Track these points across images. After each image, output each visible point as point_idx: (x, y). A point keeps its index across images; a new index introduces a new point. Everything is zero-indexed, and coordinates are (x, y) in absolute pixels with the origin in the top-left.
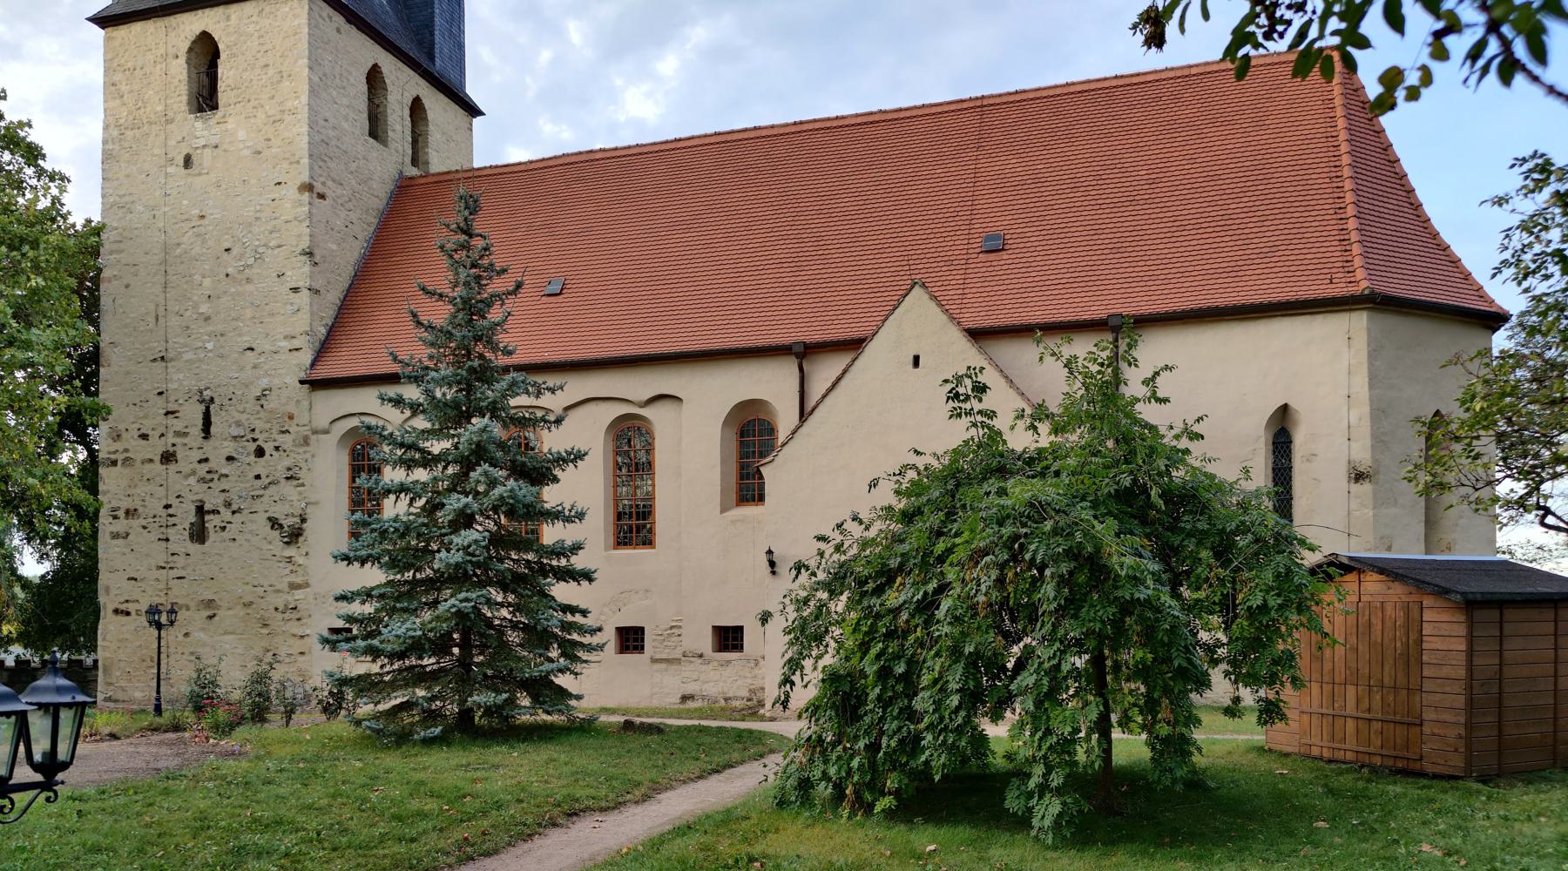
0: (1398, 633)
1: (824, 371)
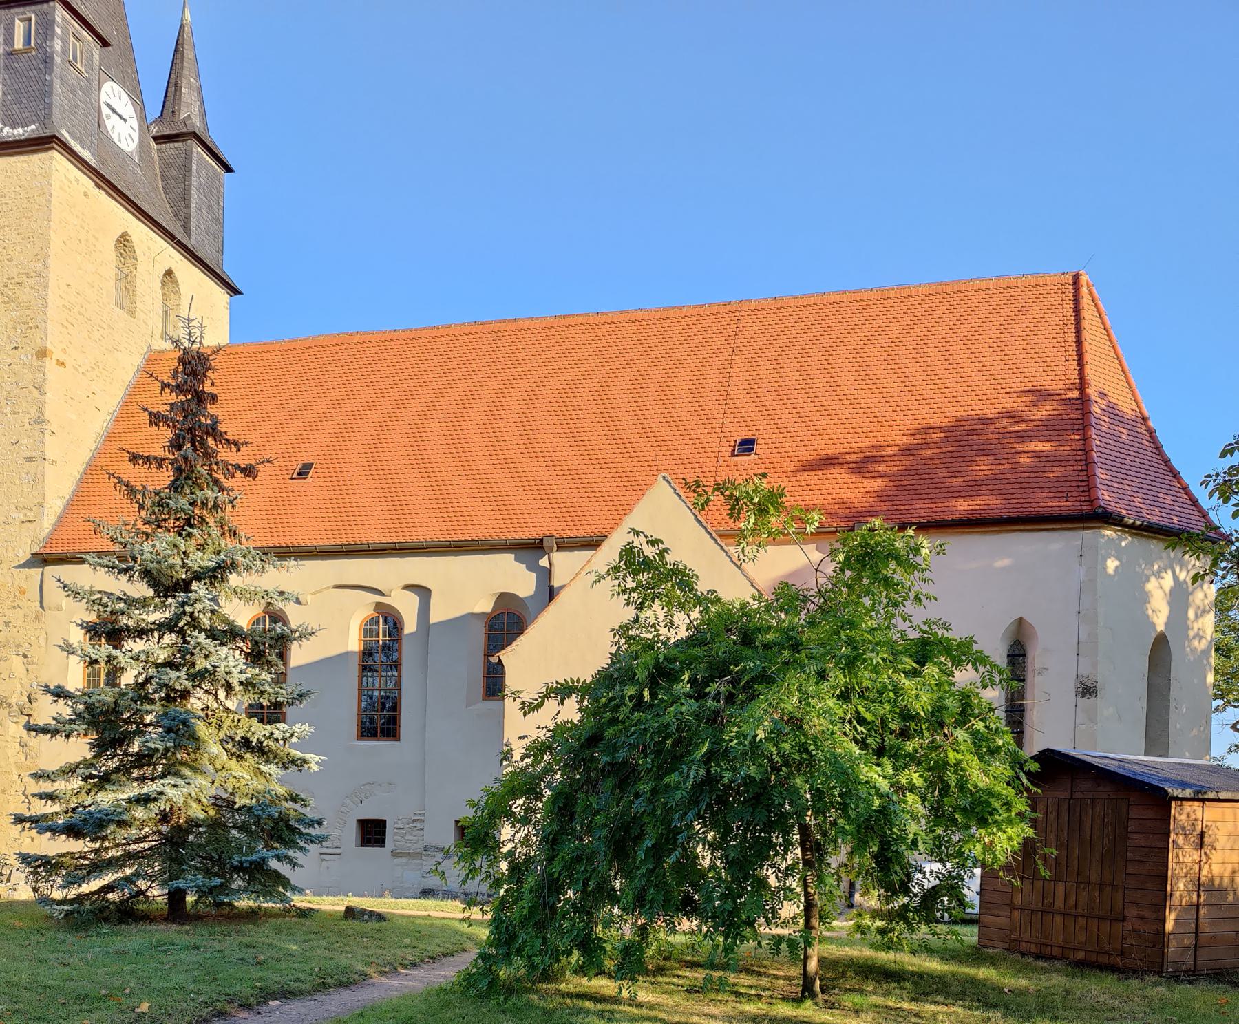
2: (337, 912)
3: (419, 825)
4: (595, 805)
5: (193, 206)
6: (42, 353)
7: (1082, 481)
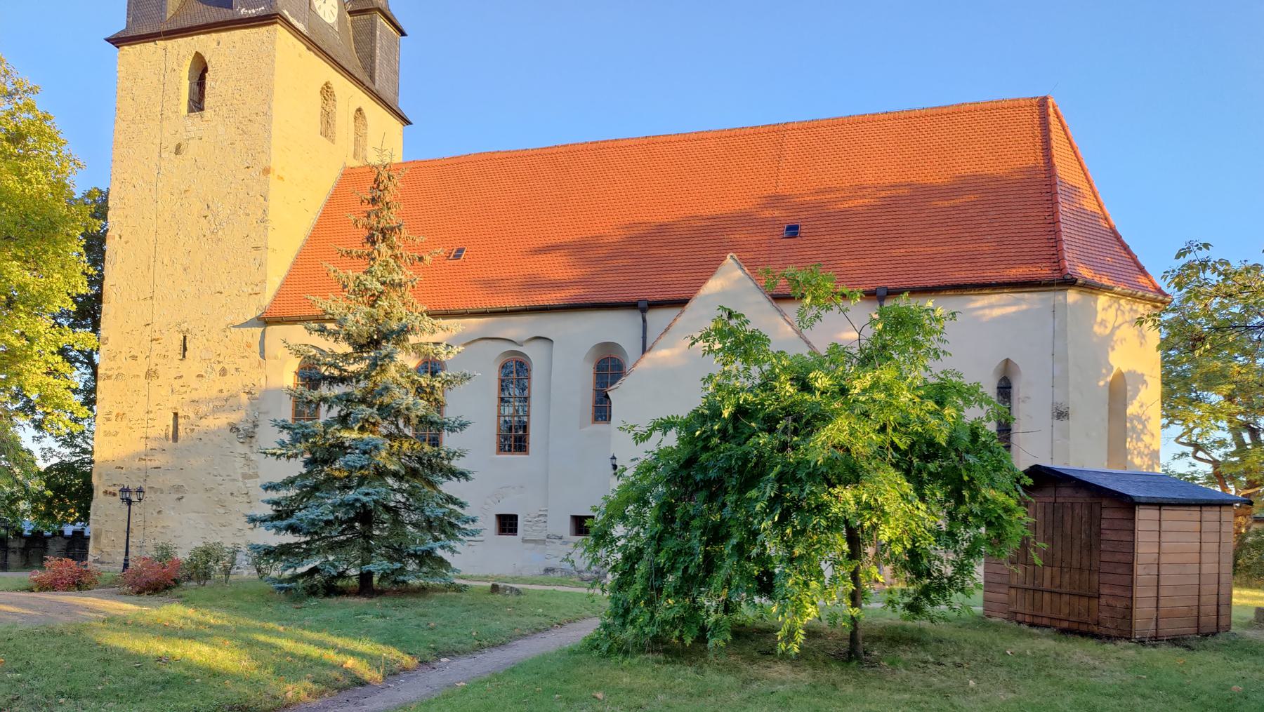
0: (1083, 528)
1: (657, 318)
2: (485, 587)
3: (542, 519)
4: (691, 512)
5: (377, 61)
6: (267, 171)
7: (1053, 254)
